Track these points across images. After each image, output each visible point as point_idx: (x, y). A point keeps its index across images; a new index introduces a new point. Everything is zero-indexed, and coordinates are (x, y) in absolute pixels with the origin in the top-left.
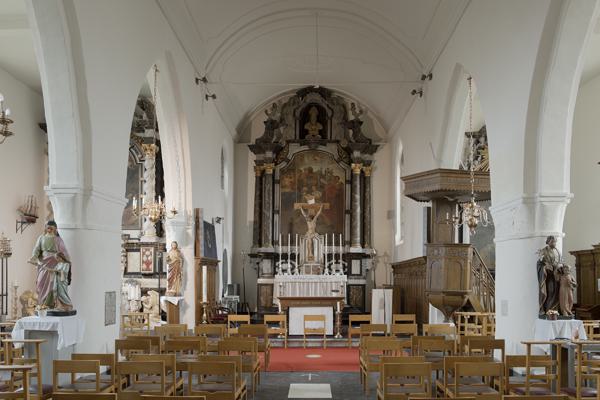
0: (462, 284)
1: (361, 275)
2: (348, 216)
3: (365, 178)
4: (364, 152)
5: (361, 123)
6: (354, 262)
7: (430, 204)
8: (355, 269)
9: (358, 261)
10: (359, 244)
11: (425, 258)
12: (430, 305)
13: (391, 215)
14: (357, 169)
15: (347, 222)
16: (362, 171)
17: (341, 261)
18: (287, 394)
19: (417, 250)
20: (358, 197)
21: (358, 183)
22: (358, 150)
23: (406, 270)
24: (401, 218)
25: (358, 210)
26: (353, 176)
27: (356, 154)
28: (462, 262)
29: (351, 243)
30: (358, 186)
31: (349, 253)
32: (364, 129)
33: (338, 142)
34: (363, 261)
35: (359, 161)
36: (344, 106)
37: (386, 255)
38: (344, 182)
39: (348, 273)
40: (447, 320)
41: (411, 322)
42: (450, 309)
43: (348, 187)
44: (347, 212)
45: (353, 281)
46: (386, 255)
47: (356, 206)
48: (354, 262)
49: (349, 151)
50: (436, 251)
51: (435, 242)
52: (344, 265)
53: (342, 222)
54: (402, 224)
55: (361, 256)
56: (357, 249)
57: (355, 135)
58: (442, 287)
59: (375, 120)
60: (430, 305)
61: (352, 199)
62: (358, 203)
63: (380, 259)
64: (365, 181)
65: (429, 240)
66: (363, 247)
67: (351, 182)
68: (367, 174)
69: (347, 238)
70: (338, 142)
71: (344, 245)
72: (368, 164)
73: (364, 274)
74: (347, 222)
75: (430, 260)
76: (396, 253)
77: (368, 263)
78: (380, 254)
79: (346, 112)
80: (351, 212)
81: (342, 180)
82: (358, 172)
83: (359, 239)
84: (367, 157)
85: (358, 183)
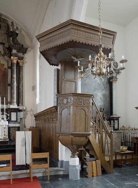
0: (86, 129)
1: (17, 121)
2: (9, 88)
3: (19, 66)
4: (18, 51)
5: (17, 34)
6: (12, 113)
7: (59, 67)
8: (14, 117)
9: (15, 113)
10: (15, 104)
11: (56, 107)
12: (60, 143)
13: (34, 88)
14: (15, 60)
15: (9, 91)
16: (18, 63)
17: (5, 113)
18: (15, 163)
19: (50, 103)
20: (15, 76)
21: (15, 68)
22: (15, 49)
23: (42, 118)
24: (40, 89)
25: (15, 84)
26: (12, 64)
27: (14, 51)
28: (86, 109)
29: (11, 103)
30: (15, 70)
31: (10, 109)
32: (18, 38)
33: (3, 44)
34: (18, 113)
35: (16, 55)
36: (8, 25)
37: (31, 110)
38: (7, 67)
39: (9, 121)
40: (73, 156)
41: (111, 38)
42: (75, 147)
43: (9, 70)
44: (9, 85)
45: (12, 125)
46: (31, 110)
47: (13, 81)
48: (12, 113)
49: (10, 49)
50: (65, 101)
51: (63, 93)
52: (7, 116)
53: (6, 91)
54: (40, 92)
55: (17, 111)
56: (15, 106)
57: (13, 40)
58: (71, 131)
59: (26, 36)
60: (60, 143)
61: (12, 77)
62: (15, 80)
63: (28, 113)
64: (20, 69)
65: (58, 92)
66: (18, 105)
67: (11, 68)
68: (21, 64)
69: (9, 100)
70: (3, 44)
71: (7, 104)
72: (22, 58)
73: (19, 120)
74: (9, 91)
75: (61, 107)
76: (36, 109)
77: (21, 115)
78: (28, 109)
79: (8, 28)
80: (11, 85)
81: (6, 66)
82: (15, 62)
83: (15, 100)
84: (21, 55)
85: (15, 68)
